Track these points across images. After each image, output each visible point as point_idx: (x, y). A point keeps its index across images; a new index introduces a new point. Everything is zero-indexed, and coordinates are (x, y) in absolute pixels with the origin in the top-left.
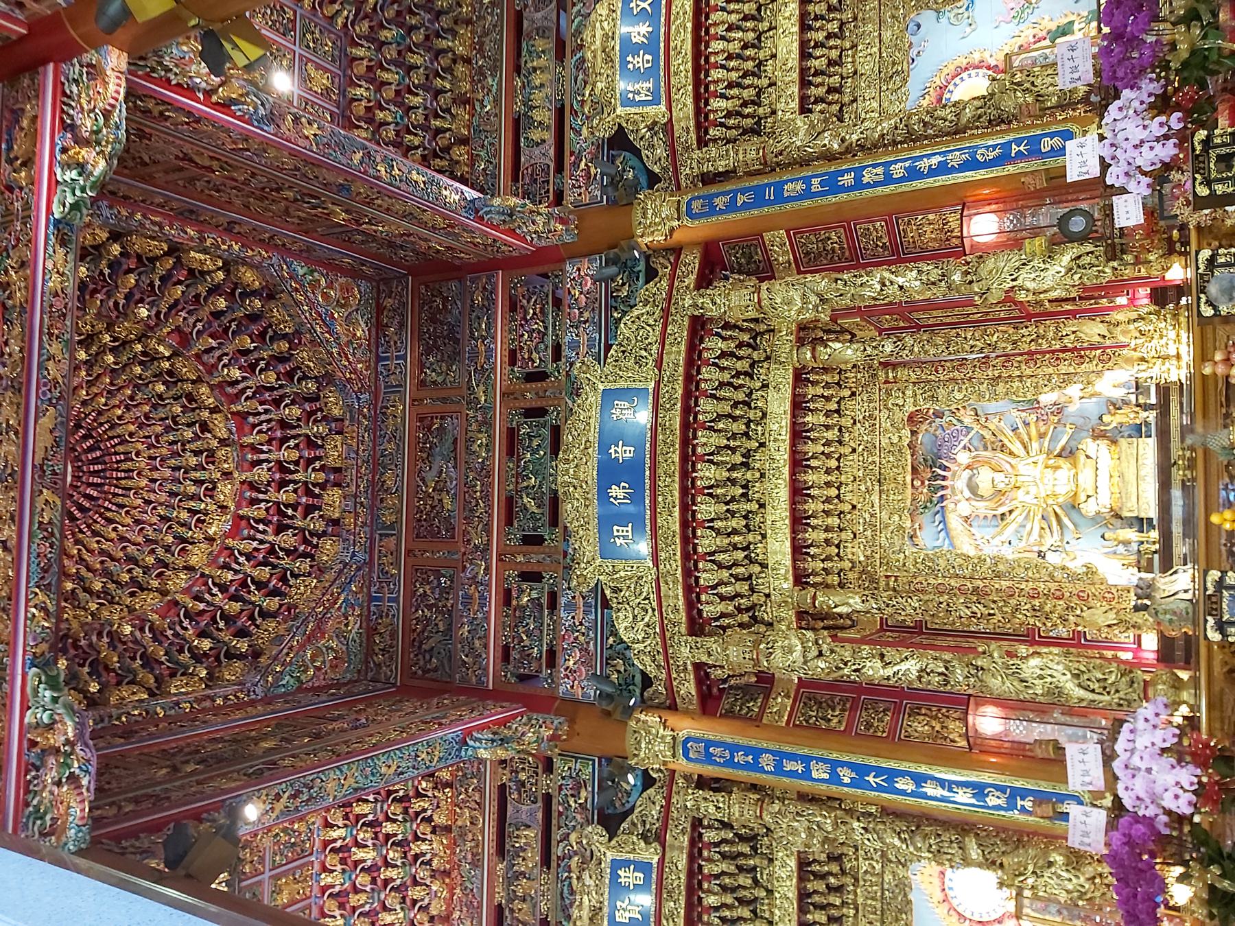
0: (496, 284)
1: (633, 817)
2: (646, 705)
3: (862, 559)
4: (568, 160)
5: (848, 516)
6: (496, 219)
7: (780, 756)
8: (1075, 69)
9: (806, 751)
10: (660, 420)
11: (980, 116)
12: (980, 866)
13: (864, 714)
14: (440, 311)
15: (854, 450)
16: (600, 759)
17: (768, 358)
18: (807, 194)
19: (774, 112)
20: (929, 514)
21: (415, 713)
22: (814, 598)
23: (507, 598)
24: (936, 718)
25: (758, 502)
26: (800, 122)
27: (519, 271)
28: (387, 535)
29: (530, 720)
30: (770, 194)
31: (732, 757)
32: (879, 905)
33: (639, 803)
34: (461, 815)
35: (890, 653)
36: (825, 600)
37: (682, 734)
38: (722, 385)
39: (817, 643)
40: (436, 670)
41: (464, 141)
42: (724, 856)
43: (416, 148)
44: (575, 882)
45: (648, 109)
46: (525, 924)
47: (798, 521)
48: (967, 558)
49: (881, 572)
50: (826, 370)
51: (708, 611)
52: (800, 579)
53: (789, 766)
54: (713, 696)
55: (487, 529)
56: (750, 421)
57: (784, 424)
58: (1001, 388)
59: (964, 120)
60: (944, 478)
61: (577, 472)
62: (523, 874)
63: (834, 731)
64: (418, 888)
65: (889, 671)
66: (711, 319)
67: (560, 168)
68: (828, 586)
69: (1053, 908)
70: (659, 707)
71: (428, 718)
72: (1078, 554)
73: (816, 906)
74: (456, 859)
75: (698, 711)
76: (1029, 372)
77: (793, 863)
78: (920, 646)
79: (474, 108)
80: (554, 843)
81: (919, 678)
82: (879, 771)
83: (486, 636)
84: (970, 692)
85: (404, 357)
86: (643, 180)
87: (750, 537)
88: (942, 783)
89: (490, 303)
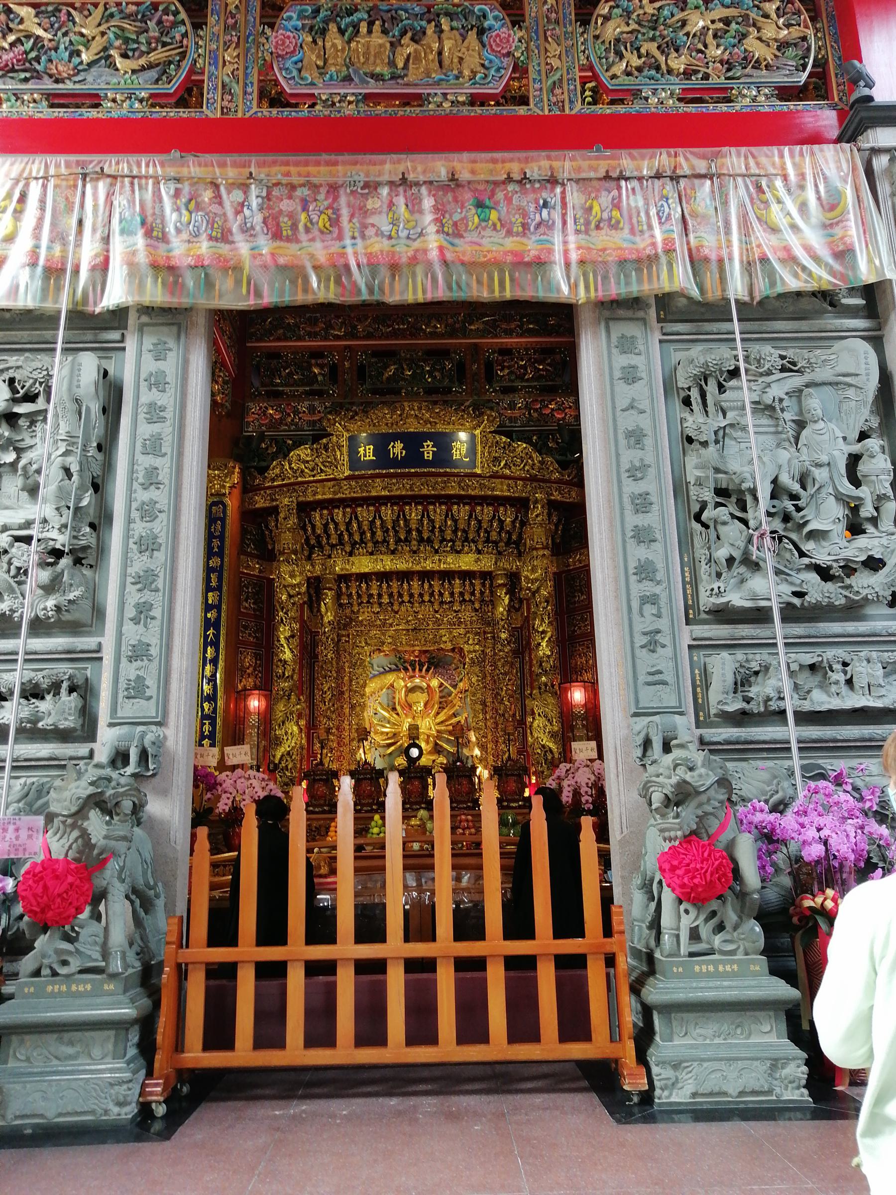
9: (225, 588)
15: (437, 612)
17: (500, 553)
20: (396, 660)
22: (330, 589)
23: (317, 354)
24: (255, 670)
25: (396, 549)
31: (215, 537)
35: (295, 641)
36: (329, 597)
37: (227, 501)
38: (480, 522)
47: (384, 576)
48: (364, 686)
50: (491, 592)
51: (317, 515)
52: (344, 578)
55: (369, 336)
58: (479, 707)
60: (420, 670)
63: (239, 603)
76: (489, 723)
78: (301, 659)
81: (280, 660)
82: (217, 636)
83: (286, 339)
87: (370, 545)
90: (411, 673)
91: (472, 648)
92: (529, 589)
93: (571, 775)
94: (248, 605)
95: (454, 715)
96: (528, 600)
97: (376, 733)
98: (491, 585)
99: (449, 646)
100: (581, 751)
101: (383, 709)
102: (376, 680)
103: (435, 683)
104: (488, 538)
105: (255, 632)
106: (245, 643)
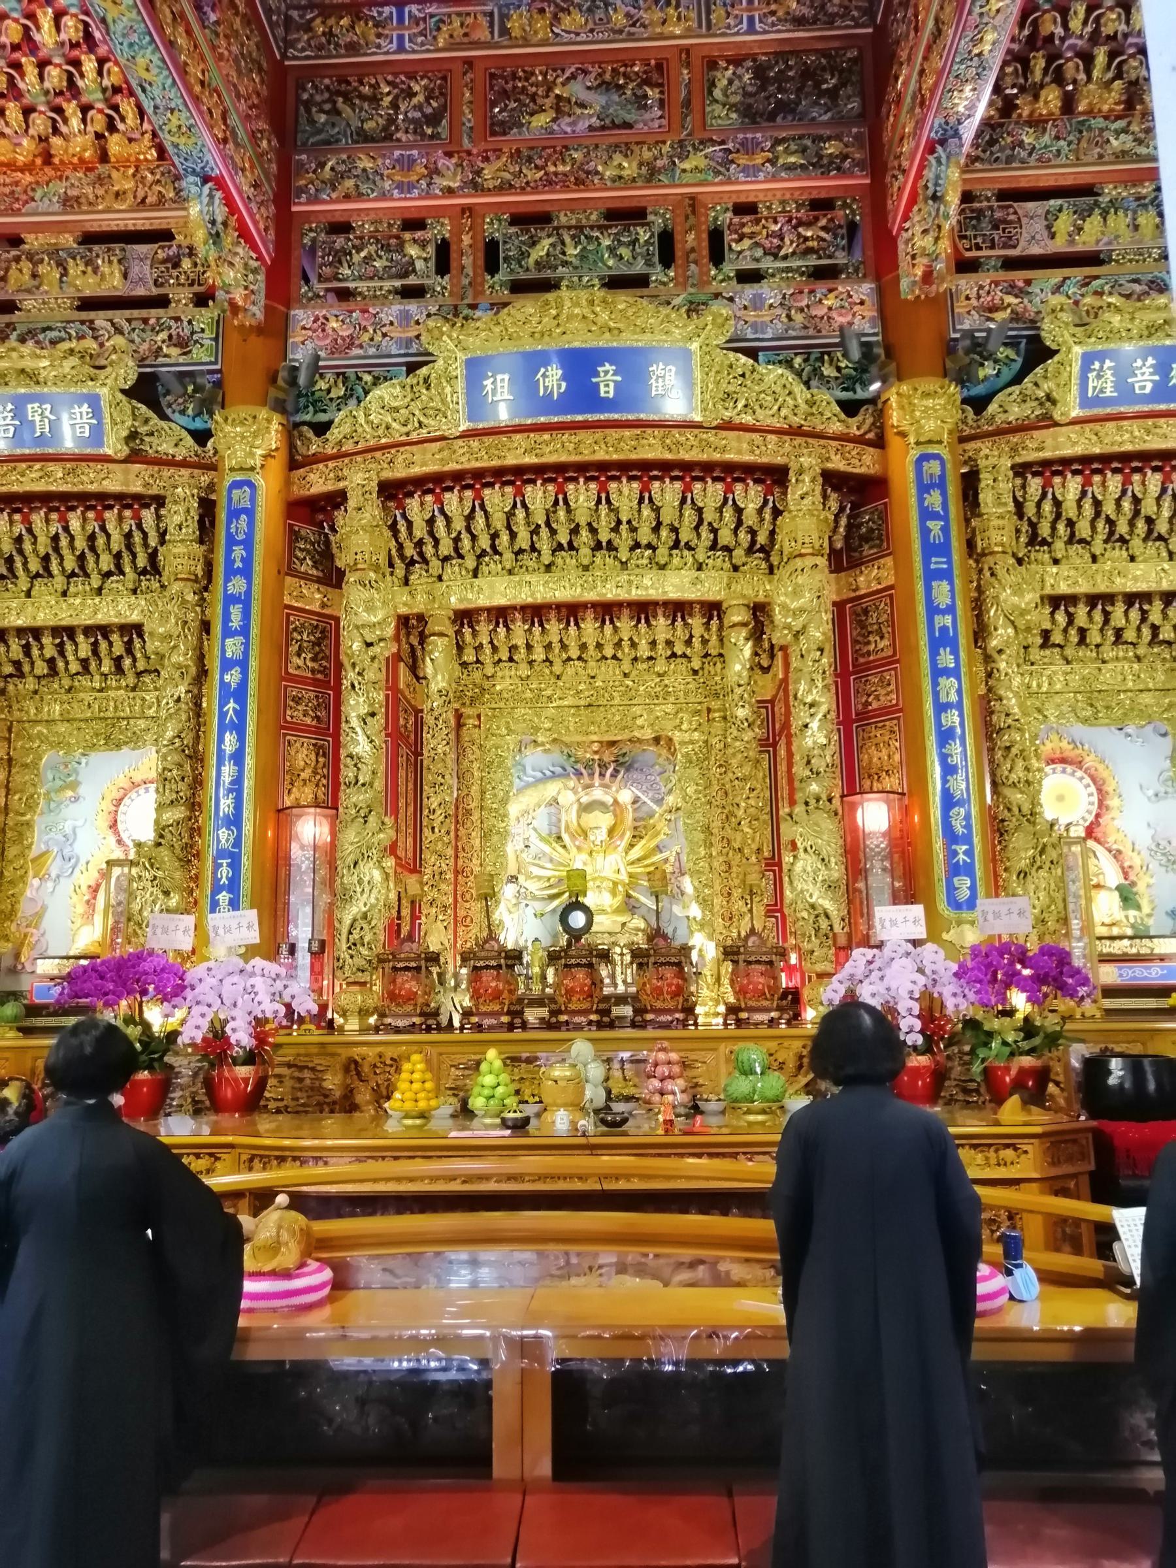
0: (852, 176)
1: (155, 419)
2: (292, 431)
3: (498, 688)
4: (1018, 277)
5: (547, 671)
6: (929, 174)
7: (245, 601)
8: (997, 915)
9: (254, 631)
10: (649, 431)
11: (1009, 810)
12: (157, 822)
13: (312, 694)
14: (817, 85)
15: (626, 675)
16: (219, 371)
18: (933, 610)
19: (1056, 562)
20: (562, 759)
21: (238, 96)
22: (441, 635)
23: (414, 224)
24: (315, 773)
26: (1030, 597)
27: (868, 210)
28: (491, 25)
29: (255, 271)
30: (938, 563)
31: (239, 543)
32: (109, 714)
33: (173, 425)
34: (125, 176)
37: (259, 480)
39: (381, 640)
40: (312, 122)
41: (1068, 104)
42: (128, 536)
43: (1065, 26)
44: (66, 345)
45: (1075, 389)
46: (3, 279)
47: (536, 613)
48: (504, 802)
49: (484, 710)
52: (465, 617)
53: (236, 612)
54: (314, 513)
56: (654, 549)
57: (651, 592)
59: (1007, 791)
60: (602, 775)
61: (578, 315)
62: (65, 273)
64: (21, 117)
65: (355, 722)
66: (785, 493)
67: (1010, 264)
68: (460, 648)
69: (122, 897)
70: (292, 448)
71: (234, 120)
72: (515, 916)
73: (95, 645)
74: (68, 173)
75: (292, 498)
76: (716, 864)
77: (135, 617)
79: (1118, 118)
80: (110, 314)
81: (351, 756)
82: (241, 714)
83: (360, 196)
84: (341, 809)
85: (751, 30)
86: (979, 390)
87: (508, 556)
88: (238, 781)
89: (821, 165)
90: (586, 780)
91: (687, 735)
92: (788, 627)
93: (875, 975)
94: (300, 664)
95: (658, 849)
96: (783, 648)
97: (529, 876)
98: (721, 628)
99: (648, 734)
100: (894, 923)
101: (542, 839)
102: (529, 792)
103: (625, 796)
104: (715, 541)
105: (314, 709)
106: (298, 728)
